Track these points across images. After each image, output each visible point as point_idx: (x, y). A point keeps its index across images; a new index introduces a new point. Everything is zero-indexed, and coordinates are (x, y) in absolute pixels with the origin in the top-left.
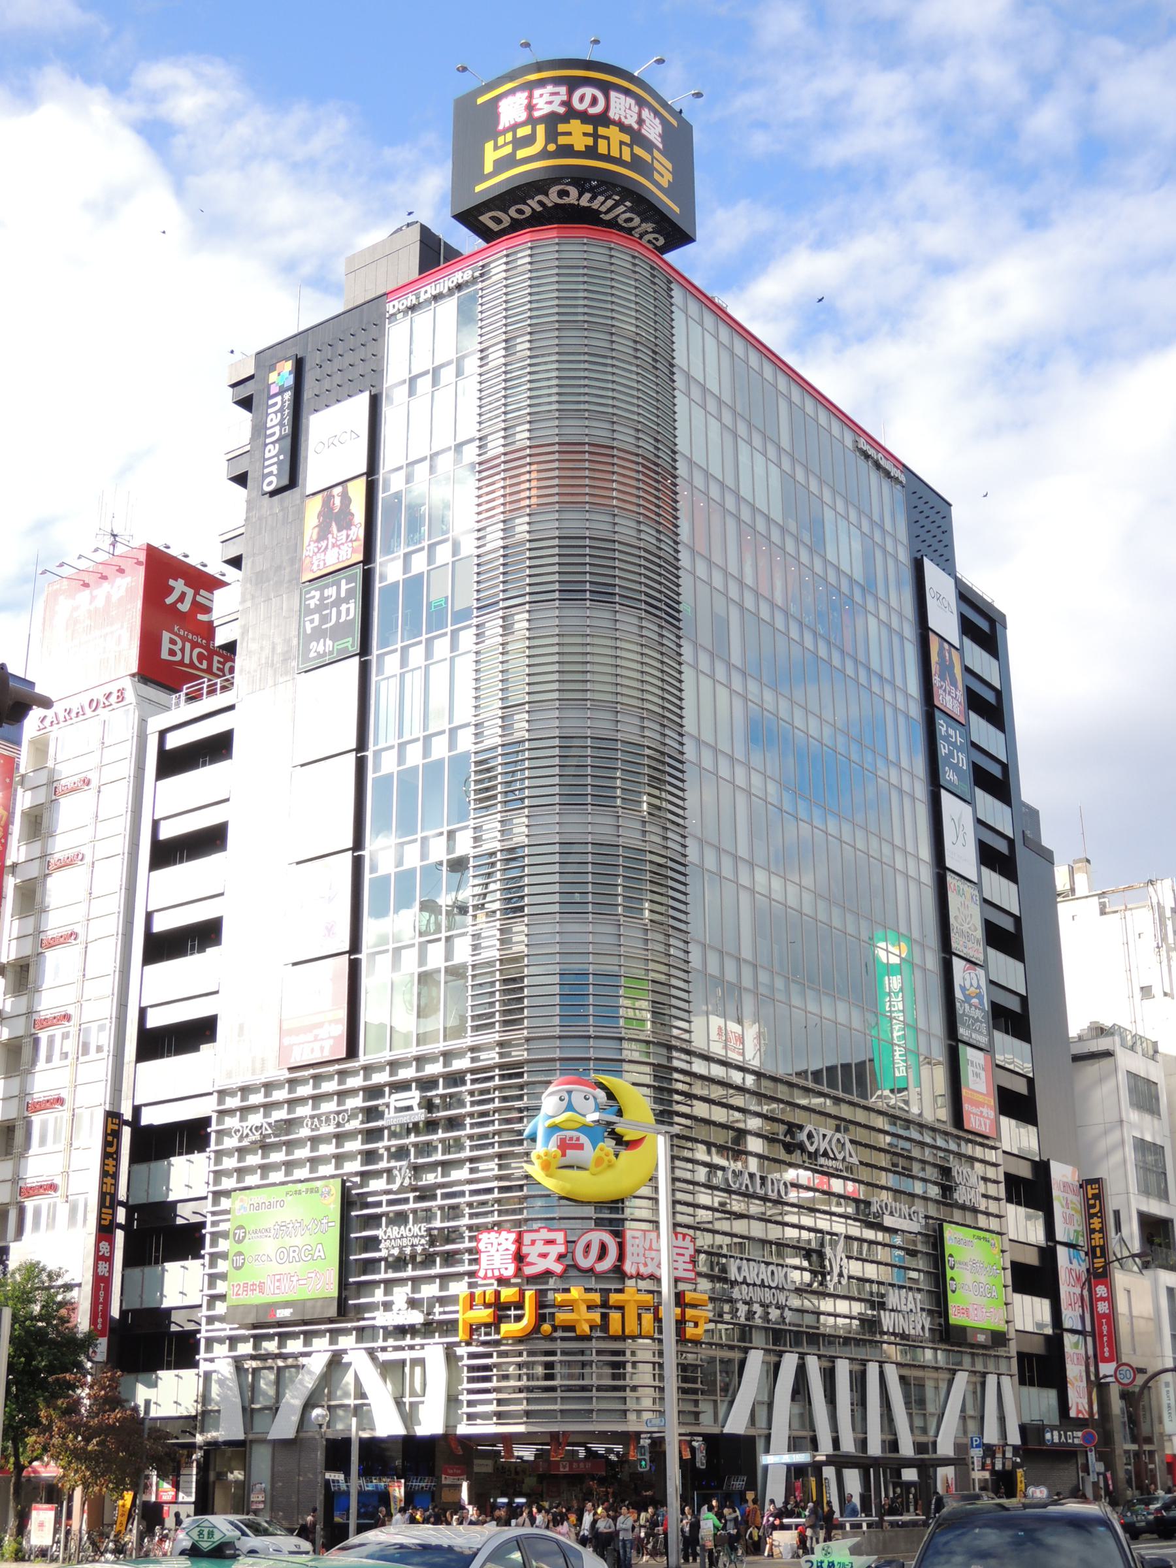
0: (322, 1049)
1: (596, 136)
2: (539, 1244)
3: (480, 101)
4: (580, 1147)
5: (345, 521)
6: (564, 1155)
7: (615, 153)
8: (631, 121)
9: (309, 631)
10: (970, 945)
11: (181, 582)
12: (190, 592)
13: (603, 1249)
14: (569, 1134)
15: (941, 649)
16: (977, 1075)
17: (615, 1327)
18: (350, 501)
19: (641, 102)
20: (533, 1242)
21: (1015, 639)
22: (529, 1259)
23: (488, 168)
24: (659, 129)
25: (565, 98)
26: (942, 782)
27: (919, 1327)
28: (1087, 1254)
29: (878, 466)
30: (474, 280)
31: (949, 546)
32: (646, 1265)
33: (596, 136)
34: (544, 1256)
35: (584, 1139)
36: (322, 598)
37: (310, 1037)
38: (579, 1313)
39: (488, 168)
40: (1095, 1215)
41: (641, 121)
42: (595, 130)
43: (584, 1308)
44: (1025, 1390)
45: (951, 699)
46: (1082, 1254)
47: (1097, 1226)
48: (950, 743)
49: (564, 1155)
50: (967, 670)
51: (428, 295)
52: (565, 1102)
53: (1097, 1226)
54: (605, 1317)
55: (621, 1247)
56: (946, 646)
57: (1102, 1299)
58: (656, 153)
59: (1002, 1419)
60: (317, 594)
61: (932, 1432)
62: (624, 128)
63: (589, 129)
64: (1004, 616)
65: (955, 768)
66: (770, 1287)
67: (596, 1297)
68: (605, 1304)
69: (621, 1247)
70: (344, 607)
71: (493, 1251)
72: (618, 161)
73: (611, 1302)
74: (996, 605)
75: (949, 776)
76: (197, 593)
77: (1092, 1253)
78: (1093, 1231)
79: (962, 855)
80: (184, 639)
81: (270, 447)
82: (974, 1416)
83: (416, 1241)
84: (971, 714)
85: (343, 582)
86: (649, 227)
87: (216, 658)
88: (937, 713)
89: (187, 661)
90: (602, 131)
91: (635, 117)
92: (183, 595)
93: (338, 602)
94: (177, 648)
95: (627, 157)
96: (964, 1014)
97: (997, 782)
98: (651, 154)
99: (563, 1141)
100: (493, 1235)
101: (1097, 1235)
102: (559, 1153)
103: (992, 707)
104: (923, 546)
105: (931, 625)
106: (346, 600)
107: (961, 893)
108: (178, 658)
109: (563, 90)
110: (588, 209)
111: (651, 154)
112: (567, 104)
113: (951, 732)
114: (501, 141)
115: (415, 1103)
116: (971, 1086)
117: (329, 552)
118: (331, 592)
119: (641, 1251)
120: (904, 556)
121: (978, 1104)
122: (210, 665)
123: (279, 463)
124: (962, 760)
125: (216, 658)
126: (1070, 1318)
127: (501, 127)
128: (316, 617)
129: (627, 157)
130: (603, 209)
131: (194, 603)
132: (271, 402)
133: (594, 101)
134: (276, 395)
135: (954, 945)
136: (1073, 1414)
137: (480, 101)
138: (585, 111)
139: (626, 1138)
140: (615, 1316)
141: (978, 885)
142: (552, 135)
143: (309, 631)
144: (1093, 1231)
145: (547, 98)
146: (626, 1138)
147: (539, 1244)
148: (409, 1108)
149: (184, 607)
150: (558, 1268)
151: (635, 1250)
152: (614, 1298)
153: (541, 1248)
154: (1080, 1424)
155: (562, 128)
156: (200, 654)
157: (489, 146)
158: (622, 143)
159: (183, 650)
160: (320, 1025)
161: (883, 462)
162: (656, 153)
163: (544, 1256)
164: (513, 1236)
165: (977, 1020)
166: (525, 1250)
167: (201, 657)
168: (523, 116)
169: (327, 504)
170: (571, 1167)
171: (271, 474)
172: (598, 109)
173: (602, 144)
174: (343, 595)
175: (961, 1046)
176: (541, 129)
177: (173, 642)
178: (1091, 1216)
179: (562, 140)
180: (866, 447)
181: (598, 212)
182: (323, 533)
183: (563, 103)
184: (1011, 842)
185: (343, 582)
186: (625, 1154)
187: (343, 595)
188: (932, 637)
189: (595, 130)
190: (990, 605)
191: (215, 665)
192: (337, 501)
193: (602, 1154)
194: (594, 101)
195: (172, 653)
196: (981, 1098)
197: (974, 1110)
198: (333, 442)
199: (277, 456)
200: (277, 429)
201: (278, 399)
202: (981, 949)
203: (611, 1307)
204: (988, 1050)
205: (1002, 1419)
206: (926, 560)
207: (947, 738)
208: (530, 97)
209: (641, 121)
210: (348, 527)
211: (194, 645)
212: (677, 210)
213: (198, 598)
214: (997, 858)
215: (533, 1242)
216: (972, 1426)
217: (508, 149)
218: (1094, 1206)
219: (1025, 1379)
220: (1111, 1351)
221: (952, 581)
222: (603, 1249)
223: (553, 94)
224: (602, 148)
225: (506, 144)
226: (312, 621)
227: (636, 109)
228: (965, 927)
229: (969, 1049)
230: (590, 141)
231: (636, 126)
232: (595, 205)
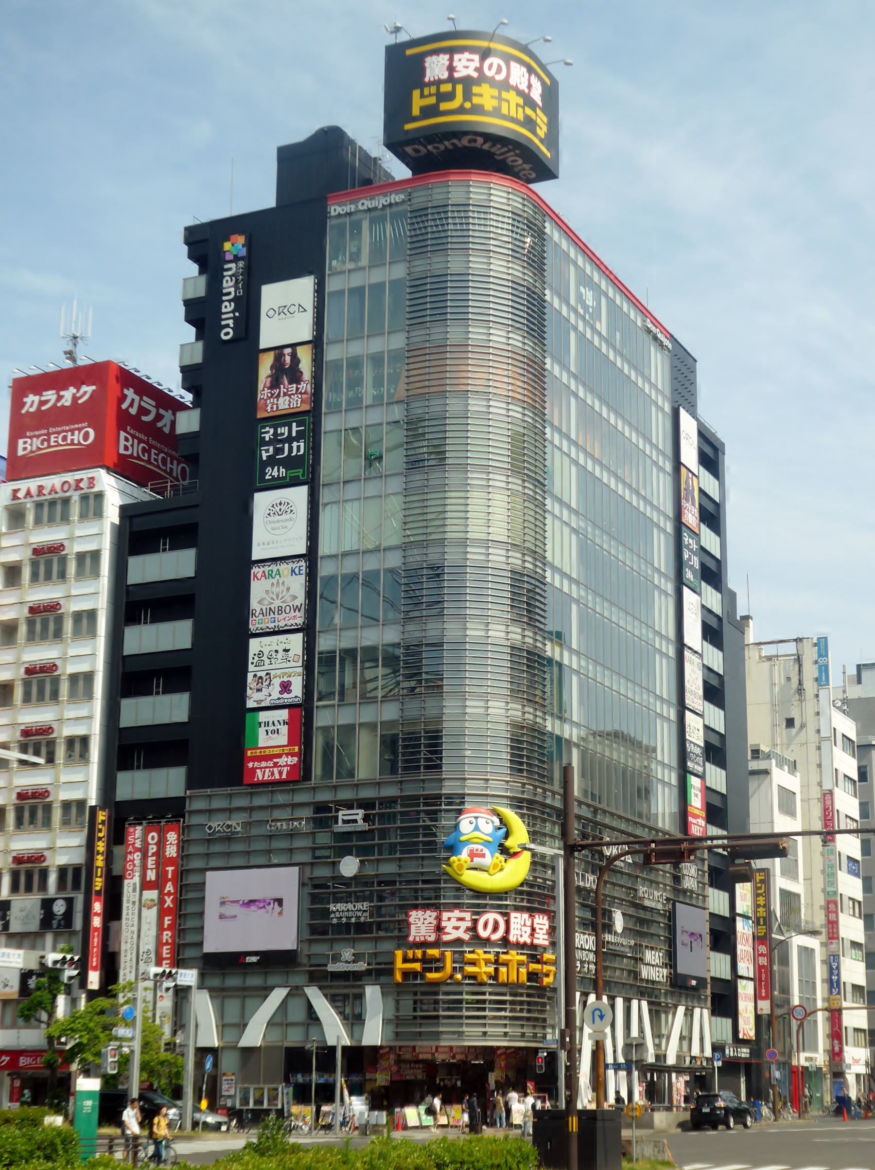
0: (280, 773)
1: (500, 98)
2: (453, 920)
3: (409, 52)
4: (483, 856)
5: (295, 376)
6: (472, 861)
7: (513, 113)
8: (523, 87)
9: (264, 458)
10: (695, 700)
11: (131, 390)
12: (137, 398)
13: (496, 923)
14: (475, 846)
15: (688, 477)
16: (696, 795)
17: (503, 978)
18: (299, 361)
19: (530, 70)
20: (449, 919)
21: (730, 462)
22: (446, 930)
23: (416, 112)
24: (540, 91)
25: (478, 65)
26: (685, 580)
27: (661, 975)
28: (753, 922)
29: (655, 338)
30: (403, 202)
31: (694, 394)
32: (521, 936)
33: (500, 98)
34: (457, 928)
35: (486, 851)
36: (275, 434)
37: (270, 764)
38: (480, 968)
39: (416, 112)
40: (761, 894)
41: (530, 86)
42: (500, 94)
43: (483, 963)
44: (714, 1018)
45: (691, 517)
46: (750, 922)
47: (762, 903)
48: (691, 550)
49: (472, 861)
50: (700, 490)
51: (365, 207)
52: (474, 825)
53: (762, 903)
54: (496, 970)
55: (507, 923)
56: (690, 475)
57: (762, 955)
58: (538, 110)
59: (702, 1039)
60: (272, 431)
61: (663, 1047)
62: (520, 93)
63: (495, 92)
64: (723, 444)
65: (691, 567)
66: (585, 950)
67: (491, 957)
68: (496, 962)
69: (507, 923)
70: (295, 444)
71: (420, 924)
73: (500, 961)
74: (719, 435)
75: (689, 575)
76: (141, 399)
77: (757, 922)
78: (758, 906)
79: (693, 635)
80: (133, 437)
81: (227, 303)
82: (686, 1038)
83: (360, 914)
84: (702, 525)
85: (294, 424)
86: (527, 166)
87: (153, 451)
88: (684, 528)
89: (135, 454)
90: (505, 95)
91: (526, 84)
92: (133, 400)
93: (290, 440)
94: (129, 444)
95: (521, 117)
96: (691, 752)
97: (713, 574)
98: (535, 111)
99: (471, 851)
100: (420, 913)
101: (761, 909)
102: (469, 859)
103: (712, 516)
104: (681, 400)
105: (682, 460)
106: (297, 439)
107: (692, 663)
108: (129, 453)
109: (476, 58)
110: (488, 152)
111: (535, 111)
112: (479, 70)
113: (691, 541)
114: (426, 91)
115: (359, 818)
116: (693, 804)
117: (281, 400)
118: (285, 430)
119: (519, 926)
120: (667, 408)
121: (696, 817)
122: (149, 457)
123: (234, 318)
124: (695, 562)
125: (153, 451)
126: (745, 967)
127: (427, 80)
128: (271, 449)
130: (498, 152)
131: (140, 407)
132: (226, 267)
133: (499, 70)
134: (230, 262)
135: (687, 701)
136: (741, 1036)
137: (409, 52)
138: (493, 78)
139: (512, 851)
140: (503, 970)
141: (701, 656)
143: (264, 458)
144: (758, 906)
145: (464, 63)
146: (512, 851)
147: (453, 920)
148: (355, 821)
149: (133, 411)
150: (466, 937)
151: (516, 926)
152: (503, 957)
153: (454, 922)
154: (745, 1042)
156: (143, 448)
157: (416, 93)
158: (517, 105)
159: (132, 445)
160: (279, 756)
161: (659, 336)
162: (538, 110)
163: (457, 928)
164: (434, 914)
165: (697, 755)
166: (443, 924)
167: (144, 450)
168: (445, 75)
169: (279, 358)
170: (475, 869)
171: (228, 326)
172: (500, 77)
173: (504, 106)
174: (294, 434)
175: (688, 775)
177: (126, 439)
178: (758, 895)
180: (650, 325)
181: (494, 154)
182: (275, 383)
183: (476, 70)
184: (720, 619)
185: (294, 424)
186: (512, 862)
187: (294, 434)
188: (683, 470)
189: (500, 94)
190: (714, 434)
191: (153, 456)
192: (288, 359)
193: (497, 861)
194: (499, 70)
195: (126, 448)
196: (697, 812)
197: (694, 821)
198: (283, 310)
199: (233, 312)
200: (232, 290)
201: (233, 265)
202: (701, 702)
203: (500, 964)
204: (702, 777)
205: (702, 1039)
206: (681, 409)
207: (687, 547)
208: (451, 60)
209: (530, 86)
210: (298, 383)
211: (160, 451)
212: (549, 155)
213: (143, 404)
214: (712, 633)
215: (449, 919)
216: (685, 1044)
217: (433, 100)
218: (760, 888)
219: (714, 1012)
220: (766, 993)
221: (695, 423)
222: (496, 923)
223: (468, 60)
224: (504, 111)
225: (430, 95)
226: (267, 451)
227: (527, 75)
228: (693, 688)
229: (693, 777)
230: (495, 103)
231: (526, 91)
232: (493, 150)
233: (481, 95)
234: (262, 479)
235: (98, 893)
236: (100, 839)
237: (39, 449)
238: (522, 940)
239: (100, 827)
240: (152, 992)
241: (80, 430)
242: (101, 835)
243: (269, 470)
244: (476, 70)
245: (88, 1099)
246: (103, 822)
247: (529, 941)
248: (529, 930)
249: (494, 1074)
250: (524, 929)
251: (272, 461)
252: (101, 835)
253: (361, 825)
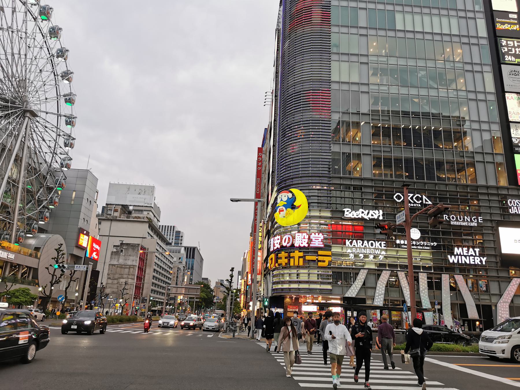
119: (301, 239)
238: (302, 245)
247: (307, 245)
248: (306, 241)
250: (303, 240)
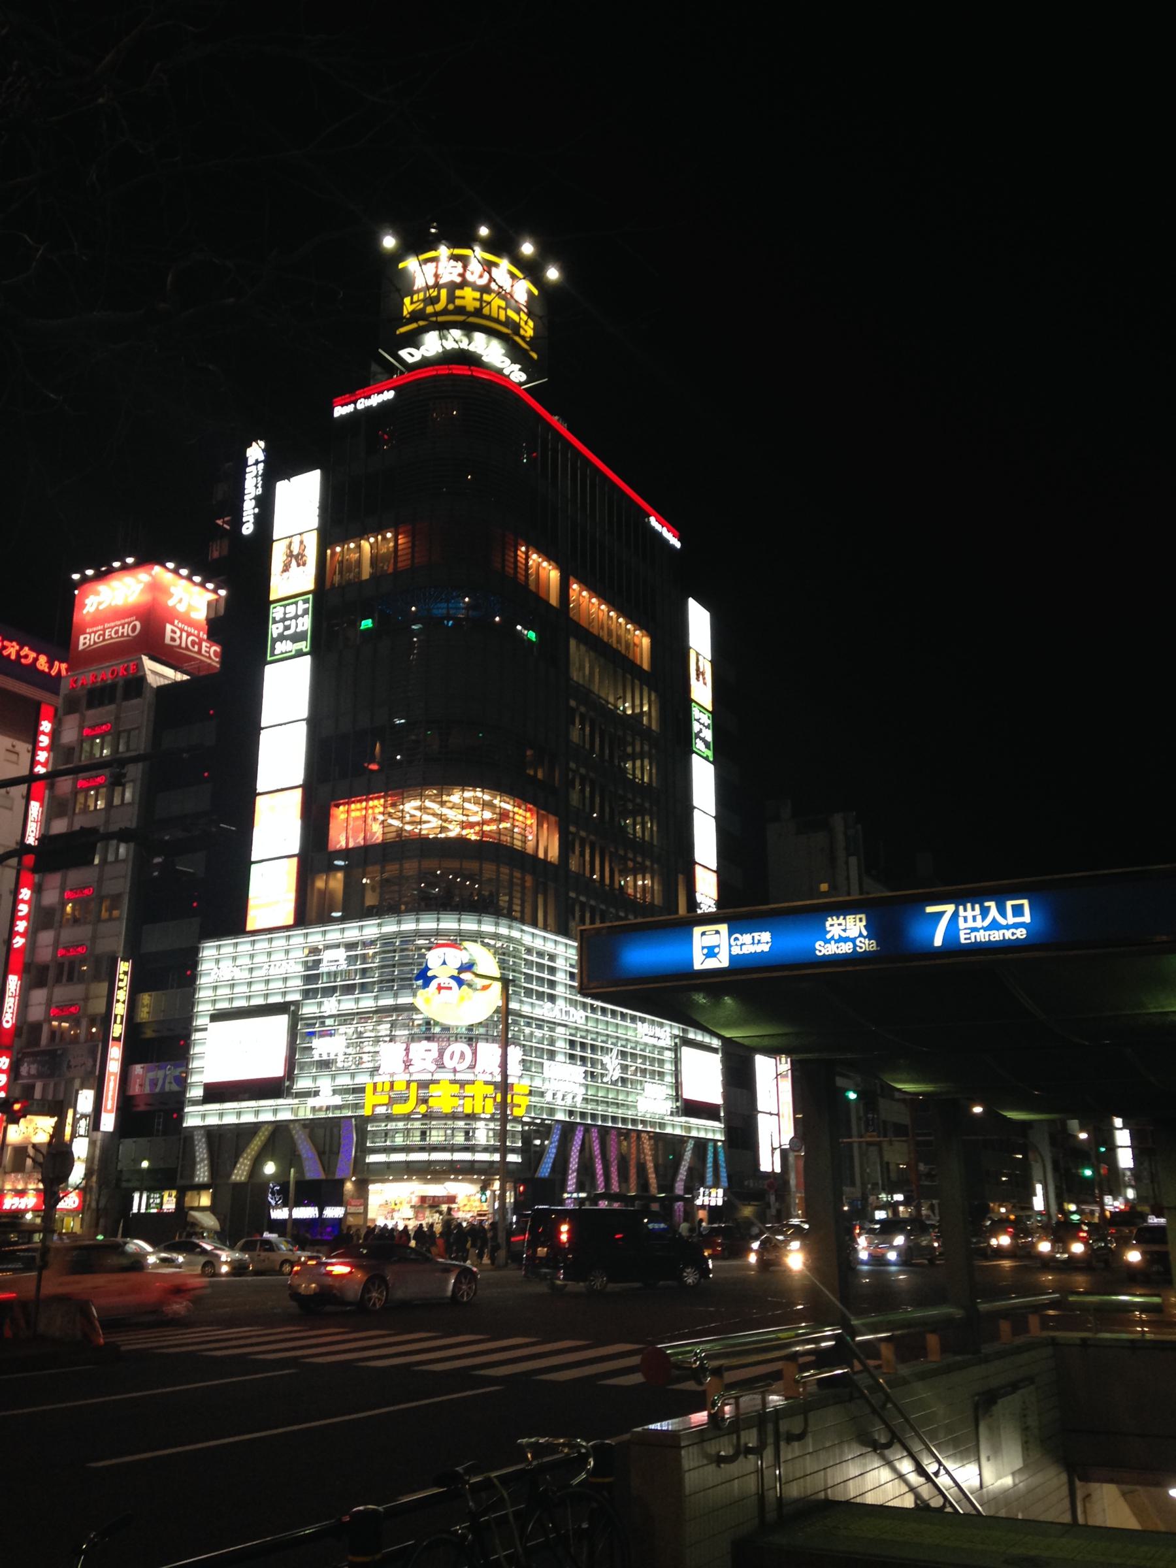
7: (494, 314)
69: (475, 1053)
72: (497, 321)
80: (182, 630)
90: (486, 297)
93: (296, 617)
112: (462, 275)
114: (415, 298)
129: (502, 317)
142: (451, 298)
155: (458, 293)
159: (181, 638)
176: (444, 292)
179: (458, 302)
183: (460, 275)
224: (486, 311)
230: (477, 304)
233: (463, 298)
234: (273, 654)
235: (117, 1039)
236: (120, 988)
237: (95, 643)
239: (122, 977)
240: (14, 872)
241: (129, 623)
242: (121, 984)
243: (278, 645)
244: (460, 275)
245: (19, 1110)
246: (125, 973)
249: (200, 614)
251: (282, 637)
252: (121, 984)
253: (343, 966)
